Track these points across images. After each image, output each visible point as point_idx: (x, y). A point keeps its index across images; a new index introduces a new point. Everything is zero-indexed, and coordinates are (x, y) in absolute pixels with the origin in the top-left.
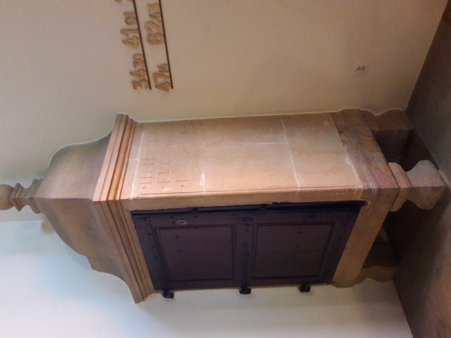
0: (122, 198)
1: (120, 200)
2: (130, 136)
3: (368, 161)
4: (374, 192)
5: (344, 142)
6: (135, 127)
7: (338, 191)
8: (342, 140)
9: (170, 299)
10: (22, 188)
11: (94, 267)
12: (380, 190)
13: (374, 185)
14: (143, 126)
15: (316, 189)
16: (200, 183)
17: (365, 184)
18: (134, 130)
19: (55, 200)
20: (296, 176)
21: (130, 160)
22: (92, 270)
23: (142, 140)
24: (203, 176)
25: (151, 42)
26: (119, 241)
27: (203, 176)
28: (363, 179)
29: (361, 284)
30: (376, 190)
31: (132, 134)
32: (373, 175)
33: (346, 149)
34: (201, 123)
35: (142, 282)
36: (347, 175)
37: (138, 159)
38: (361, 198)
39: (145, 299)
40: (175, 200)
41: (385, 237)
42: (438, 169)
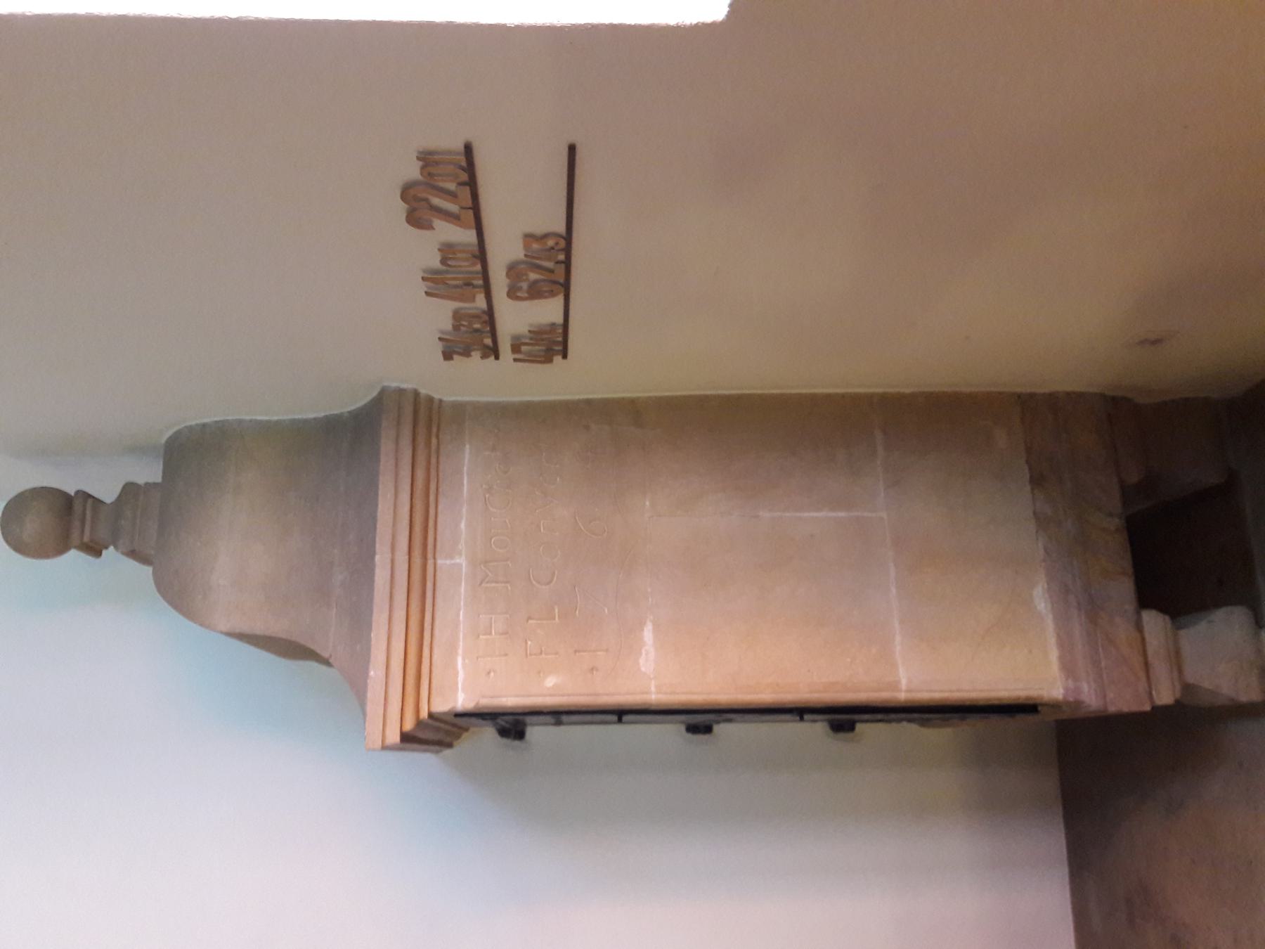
1: (431, 715)
3: (1093, 610)
5: (1042, 522)
8: (1035, 513)
9: (517, 743)
10: (97, 501)
13: (1093, 697)
16: (642, 661)
17: (1071, 683)
18: (437, 437)
20: (898, 648)
21: (439, 562)
24: (648, 634)
25: (512, 294)
27: (648, 634)
28: (1068, 668)
31: (433, 460)
33: (1042, 552)
36: (1030, 652)
37: (461, 560)
42: (1261, 627)
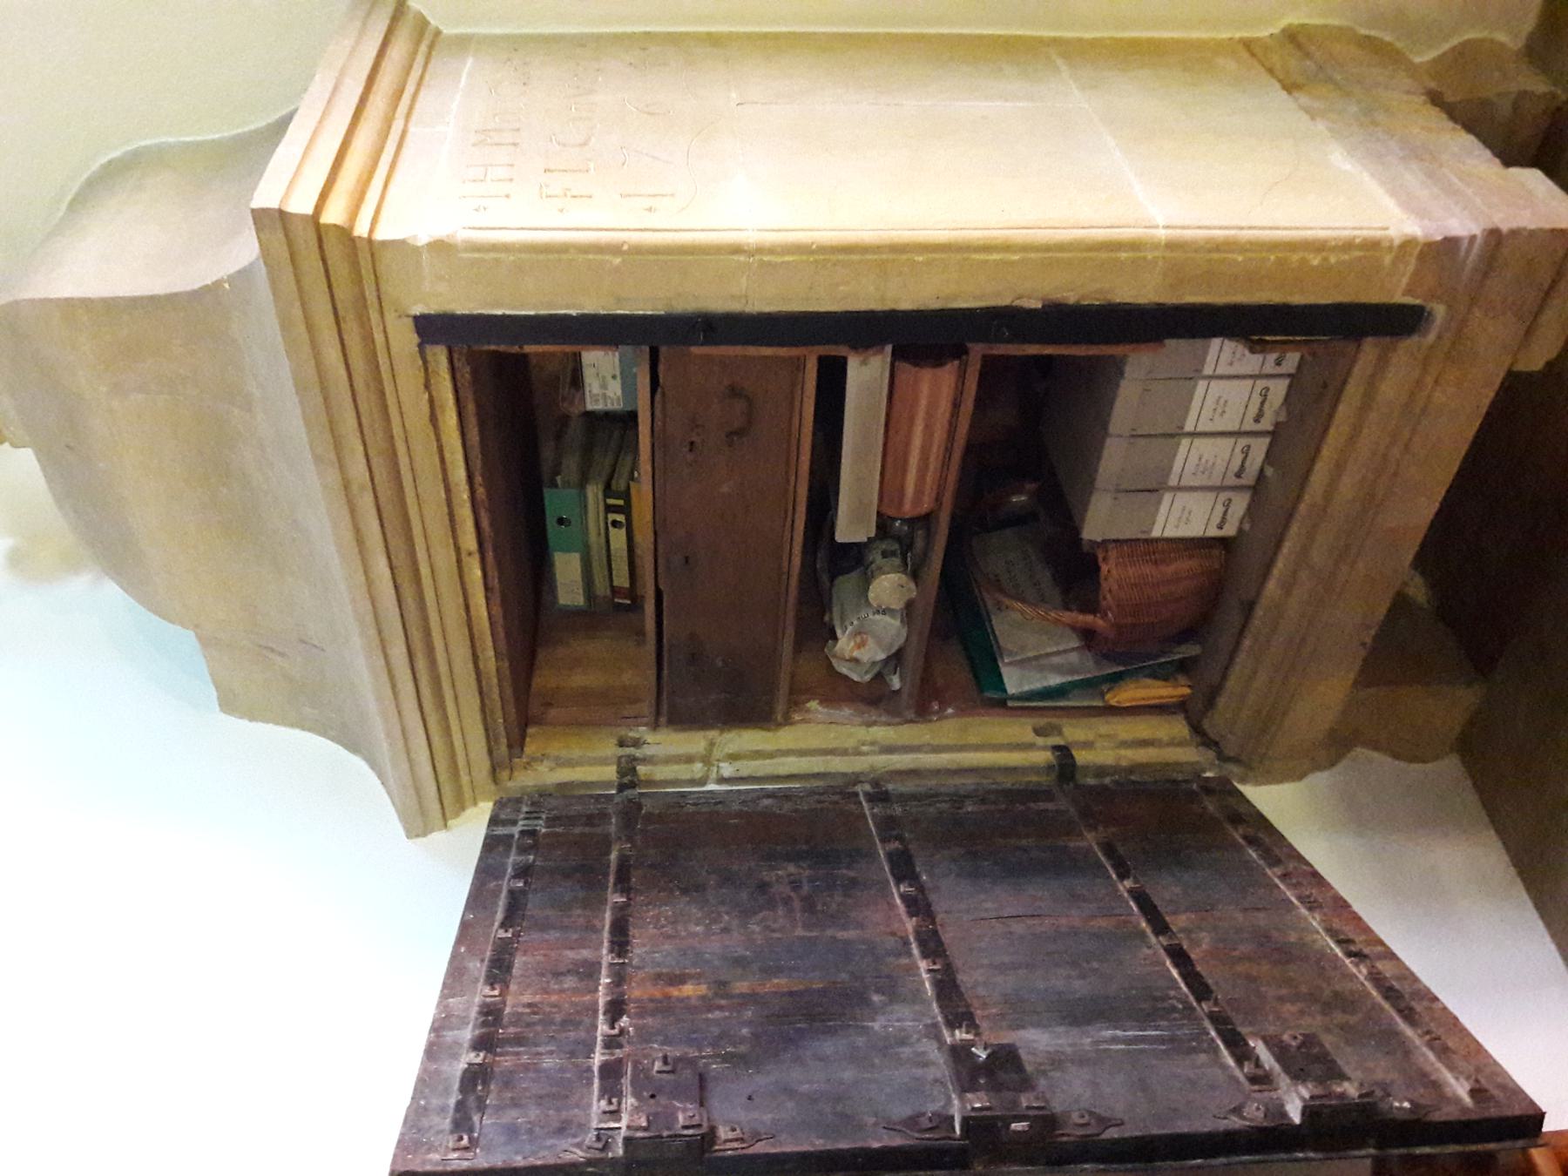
0: (379, 236)
2: (408, 69)
4: (1468, 251)
5: (1312, 114)
6: (431, 47)
7: (1319, 246)
11: (230, 703)
12: (1495, 237)
14: (463, 43)
15: (1233, 232)
19: (71, 308)
22: (223, 716)
23: (463, 79)
26: (358, 469)
29: (1335, 769)
30: (1479, 241)
31: (420, 59)
32: (1450, 191)
34: (715, 41)
35: (447, 731)
36: (1387, 110)
38: (1409, 291)
39: (450, 823)
40: (617, 261)
41: (1419, 591)
